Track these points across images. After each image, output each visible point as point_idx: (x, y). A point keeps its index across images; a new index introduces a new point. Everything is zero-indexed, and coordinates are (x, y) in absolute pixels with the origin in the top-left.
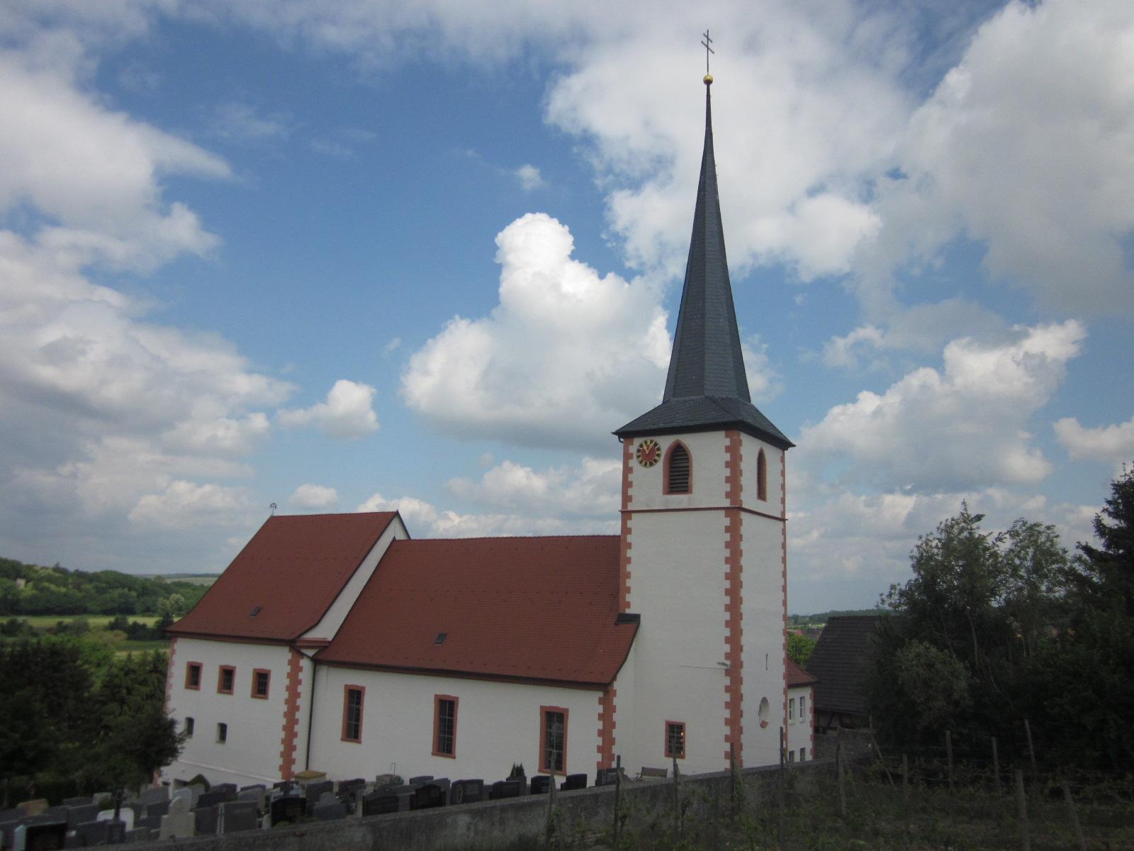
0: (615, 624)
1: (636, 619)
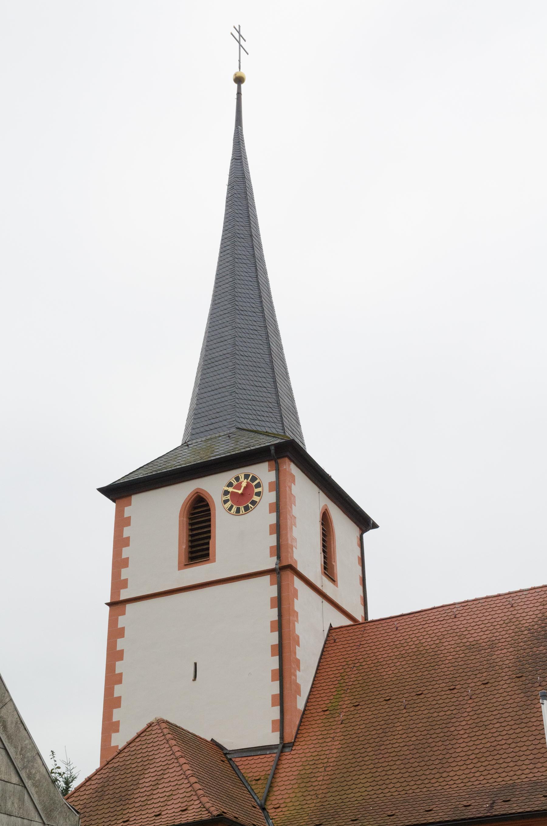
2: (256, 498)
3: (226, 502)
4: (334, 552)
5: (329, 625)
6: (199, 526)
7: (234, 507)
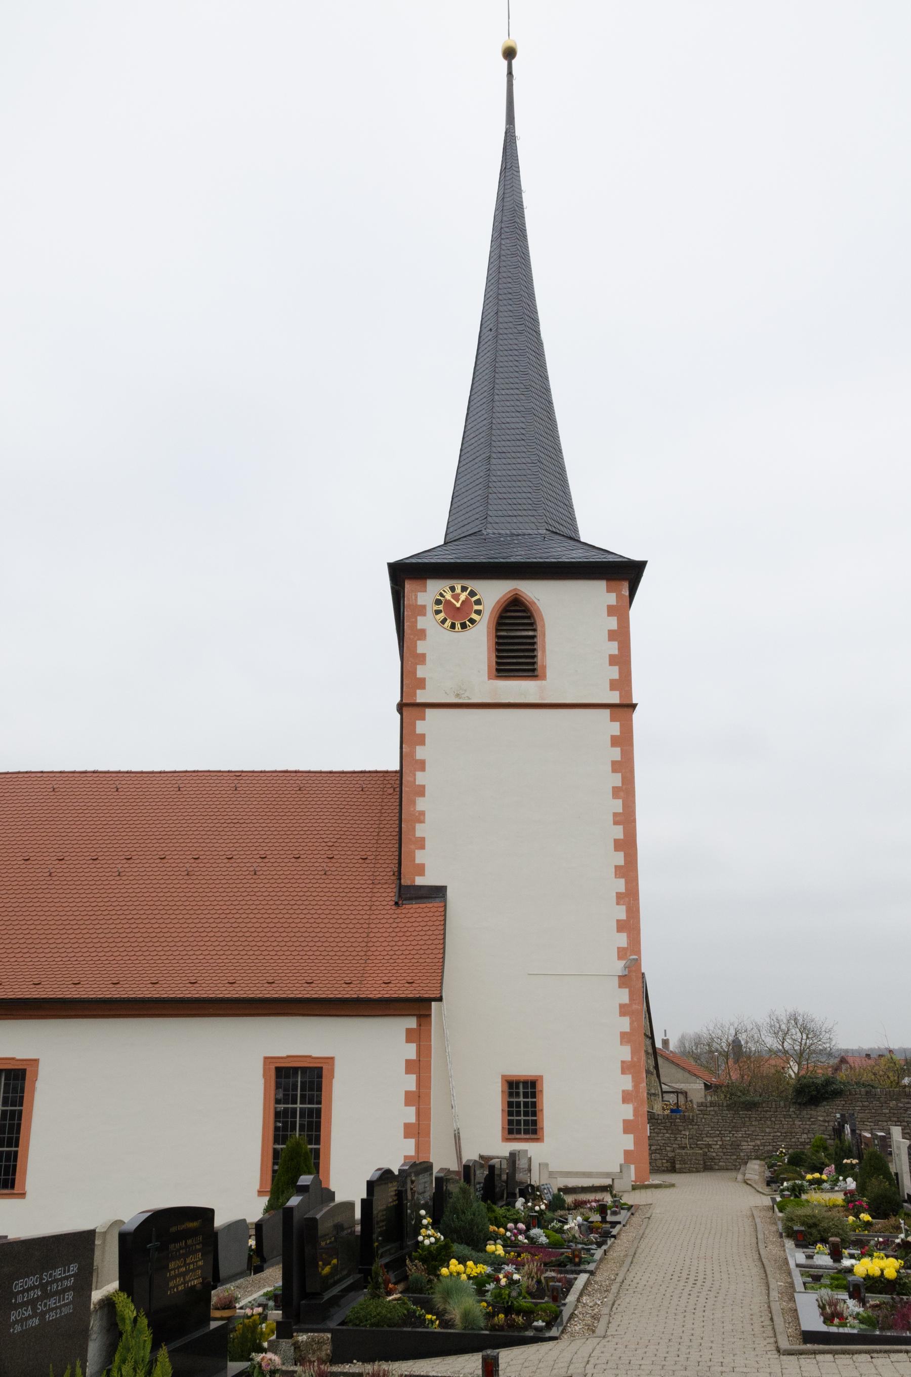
0: (396, 903)
1: (439, 893)
3: (438, 612)
4: (514, 676)
6: (515, 661)
7: (448, 621)
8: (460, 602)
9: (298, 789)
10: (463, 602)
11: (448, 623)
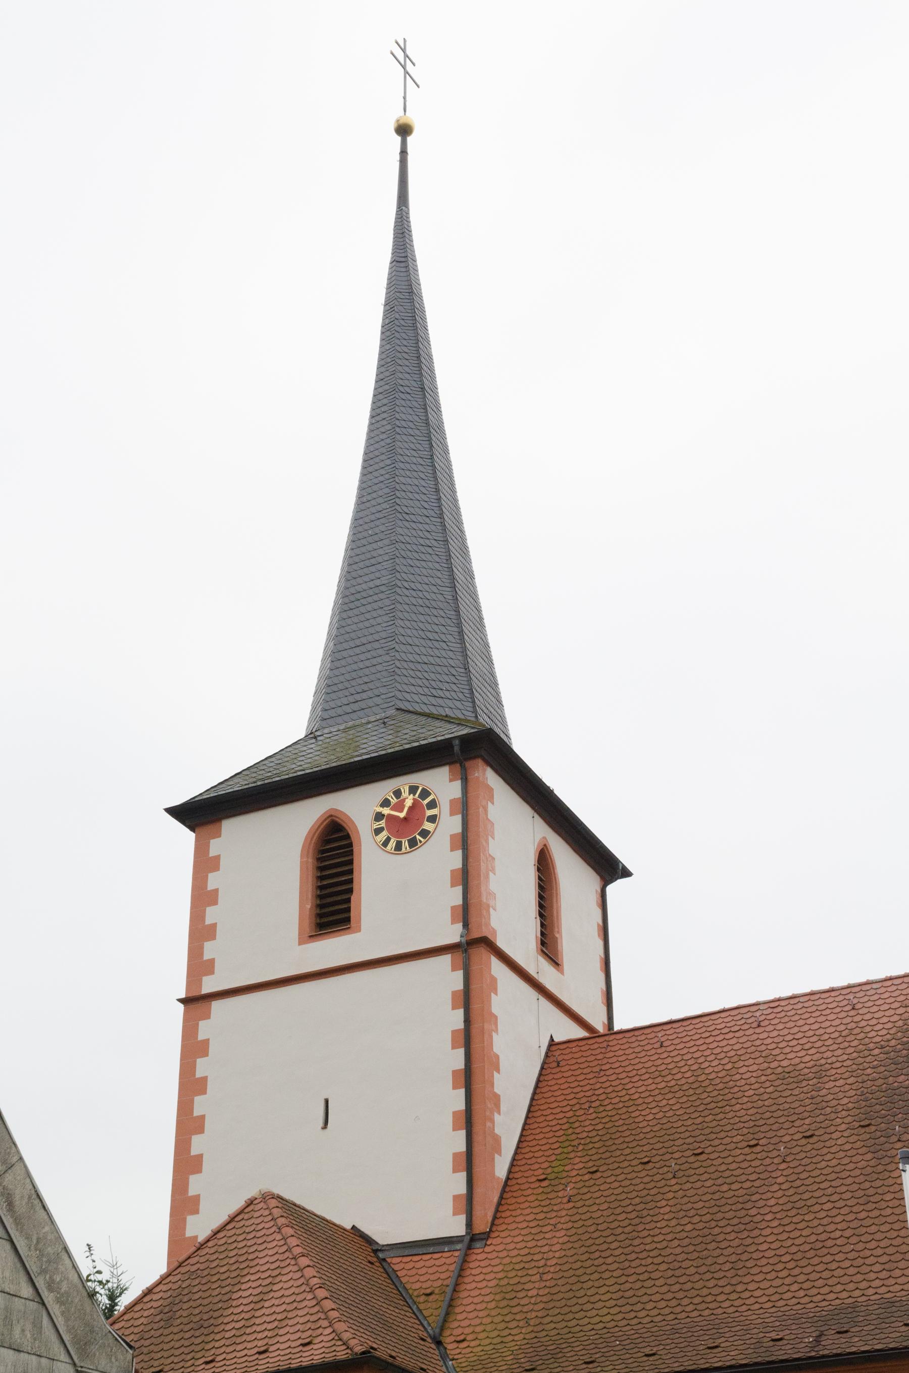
2: (428, 826)
3: (378, 831)
5: (549, 1038)
7: (392, 840)
8: (406, 810)
9: (849, 1007)
10: (410, 809)
11: (392, 844)
